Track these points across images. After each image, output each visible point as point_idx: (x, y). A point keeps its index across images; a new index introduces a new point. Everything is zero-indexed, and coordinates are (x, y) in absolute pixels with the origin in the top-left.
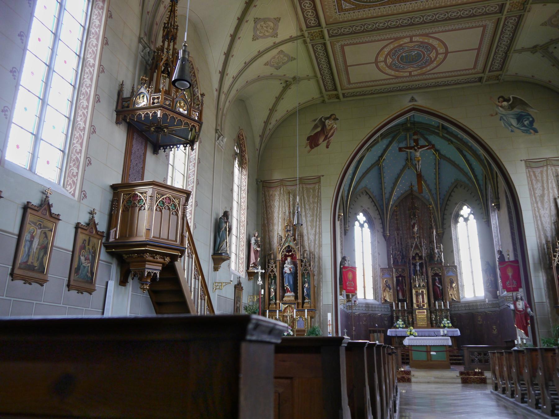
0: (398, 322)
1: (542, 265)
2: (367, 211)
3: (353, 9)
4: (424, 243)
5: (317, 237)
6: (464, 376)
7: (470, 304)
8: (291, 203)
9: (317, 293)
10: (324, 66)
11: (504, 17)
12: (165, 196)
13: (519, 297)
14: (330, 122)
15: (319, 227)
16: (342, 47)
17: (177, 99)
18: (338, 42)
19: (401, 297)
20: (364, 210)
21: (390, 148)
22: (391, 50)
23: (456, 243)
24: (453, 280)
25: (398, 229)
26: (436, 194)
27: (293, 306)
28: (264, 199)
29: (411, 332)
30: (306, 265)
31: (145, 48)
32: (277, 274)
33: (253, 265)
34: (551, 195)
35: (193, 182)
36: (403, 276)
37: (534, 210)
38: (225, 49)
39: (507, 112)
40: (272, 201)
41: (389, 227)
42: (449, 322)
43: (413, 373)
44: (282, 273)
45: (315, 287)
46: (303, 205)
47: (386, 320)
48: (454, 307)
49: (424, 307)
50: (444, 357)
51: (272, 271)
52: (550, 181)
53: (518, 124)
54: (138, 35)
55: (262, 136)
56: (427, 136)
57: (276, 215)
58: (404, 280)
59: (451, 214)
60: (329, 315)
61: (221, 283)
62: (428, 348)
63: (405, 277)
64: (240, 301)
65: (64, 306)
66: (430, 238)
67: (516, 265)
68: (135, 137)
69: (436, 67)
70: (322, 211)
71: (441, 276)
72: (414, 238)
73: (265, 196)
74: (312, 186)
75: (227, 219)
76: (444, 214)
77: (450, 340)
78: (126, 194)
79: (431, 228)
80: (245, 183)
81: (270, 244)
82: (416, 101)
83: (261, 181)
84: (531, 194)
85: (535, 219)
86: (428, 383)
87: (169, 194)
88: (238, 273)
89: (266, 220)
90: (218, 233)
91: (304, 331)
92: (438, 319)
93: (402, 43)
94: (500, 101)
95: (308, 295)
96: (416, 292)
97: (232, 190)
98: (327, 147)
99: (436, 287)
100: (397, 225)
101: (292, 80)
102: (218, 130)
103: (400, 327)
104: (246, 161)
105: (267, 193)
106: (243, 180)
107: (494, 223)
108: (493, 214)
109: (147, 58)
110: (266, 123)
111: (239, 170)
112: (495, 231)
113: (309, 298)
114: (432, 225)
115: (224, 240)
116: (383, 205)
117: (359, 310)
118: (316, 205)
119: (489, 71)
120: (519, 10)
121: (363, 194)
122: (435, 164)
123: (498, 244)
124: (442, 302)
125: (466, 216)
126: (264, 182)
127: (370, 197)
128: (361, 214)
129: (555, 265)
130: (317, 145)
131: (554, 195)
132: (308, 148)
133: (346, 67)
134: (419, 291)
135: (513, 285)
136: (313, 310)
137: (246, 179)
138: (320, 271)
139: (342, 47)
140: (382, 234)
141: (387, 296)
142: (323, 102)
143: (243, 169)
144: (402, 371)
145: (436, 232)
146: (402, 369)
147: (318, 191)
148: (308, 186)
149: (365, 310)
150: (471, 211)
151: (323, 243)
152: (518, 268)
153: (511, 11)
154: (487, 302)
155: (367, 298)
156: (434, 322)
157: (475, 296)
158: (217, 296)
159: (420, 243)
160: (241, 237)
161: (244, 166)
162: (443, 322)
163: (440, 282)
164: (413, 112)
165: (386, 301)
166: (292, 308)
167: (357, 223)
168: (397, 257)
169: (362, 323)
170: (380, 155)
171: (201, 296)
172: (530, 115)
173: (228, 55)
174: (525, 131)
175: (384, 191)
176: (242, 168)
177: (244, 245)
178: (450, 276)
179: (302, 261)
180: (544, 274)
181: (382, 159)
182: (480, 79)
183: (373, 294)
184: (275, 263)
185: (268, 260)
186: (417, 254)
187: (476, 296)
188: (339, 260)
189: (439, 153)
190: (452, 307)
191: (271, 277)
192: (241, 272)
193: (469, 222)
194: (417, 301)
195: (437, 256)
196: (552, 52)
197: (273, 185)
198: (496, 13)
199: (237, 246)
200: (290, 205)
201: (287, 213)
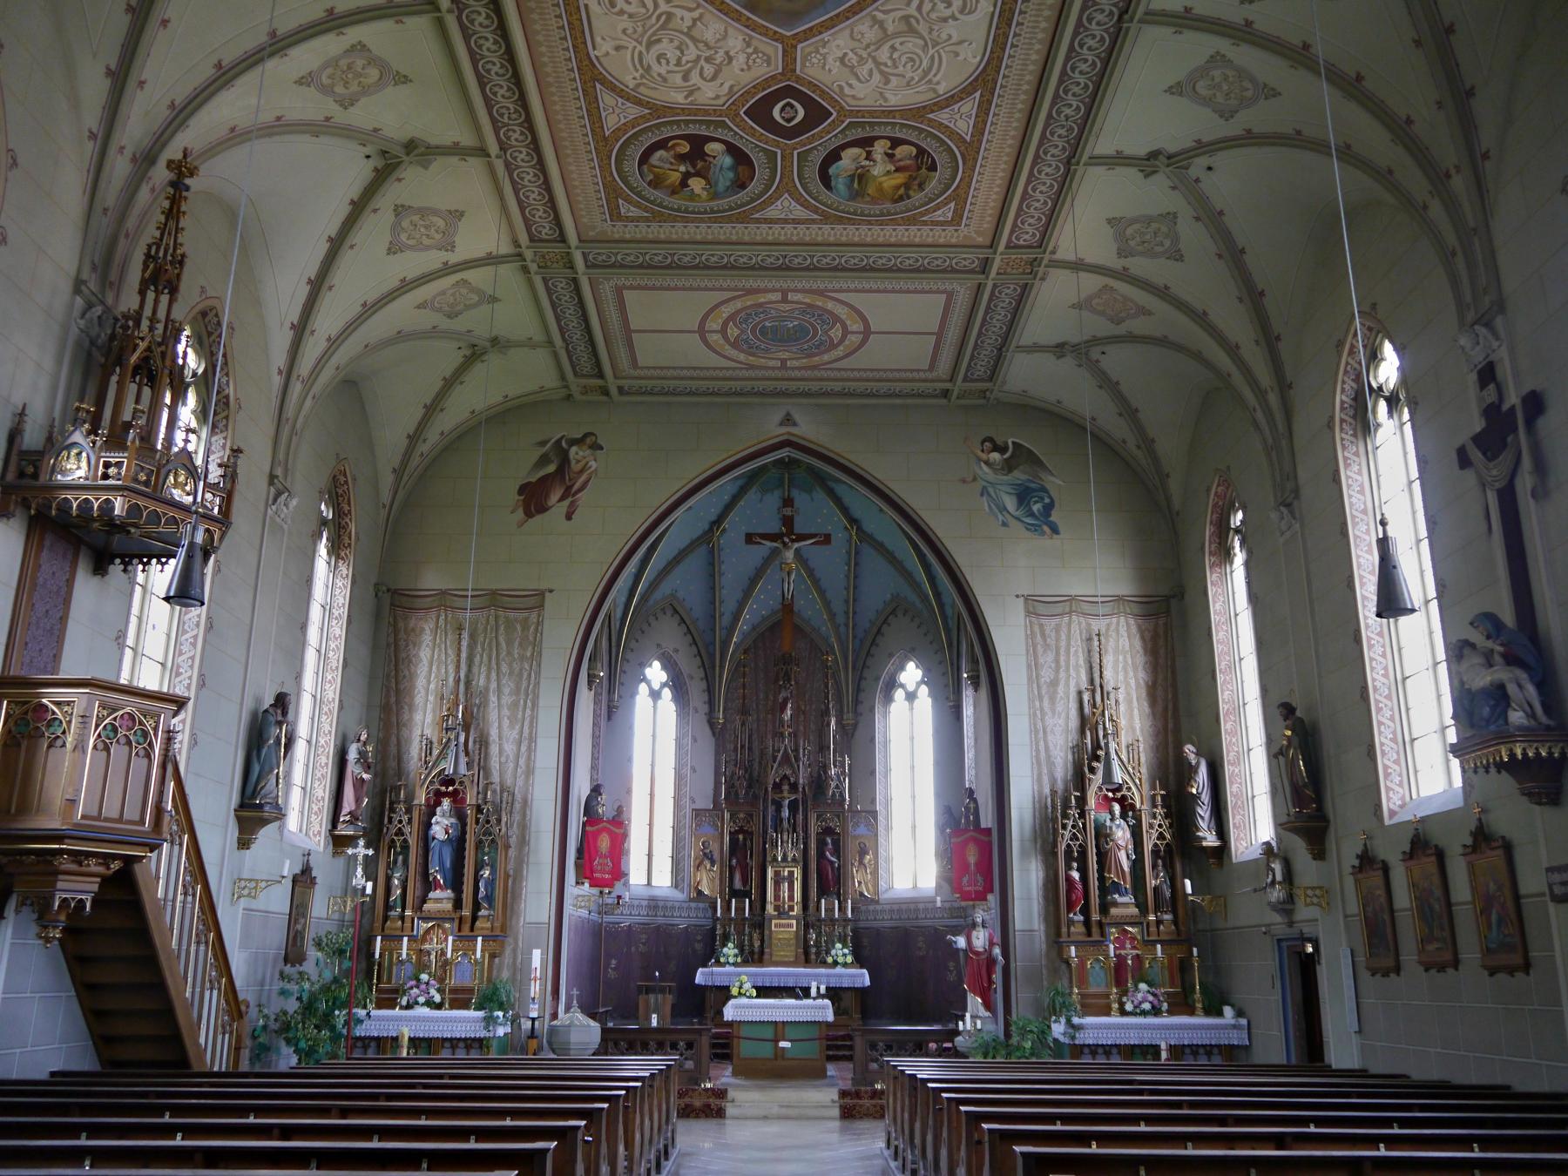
0: (725, 950)
3: (647, 220)
5: (523, 749)
6: (848, 1101)
8: (464, 655)
9: (513, 892)
10: (573, 322)
11: (990, 284)
12: (121, 713)
13: (979, 920)
14: (581, 453)
15: (531, 723)
16: (619, 291)
17: (170, 466)
18: (608, 280)
19: (738, 885)
20: (663, 654)
21: (742, 503)
22: (738, 312)
25: (744, 711)
26: (847, 625)
27: (447, 925)
28: (391, 640)
29: (740, 988)
30: (488, 822)
31: (89, 306)
32: (412, 841)
33: (347, 818)
34: (1072, 684)
35: (198, 625)
37: (1033, 716)
38: (312, 272)
40: (415, 645)
41: (725, 702)
42: (846, 951)
43: (731, 1094)
44: (426, 838)
45: (507, 876)
46: (494, 662)
47: (699, 941)
50: (813, 1050)
51: (400, 832)
52: (1072, 650)
54: (73, 270)
55: (398, 473)
57: (420, 682)
58: (748, 843)
59: (878, 679)
60: (537, 955)
61: (257, 881)
62: (779, 1029)
63: (752, 833)
64: (304, 916)
66: (820, 736)
68: (47, 543)
69: (847, 356)
70: (542, 680)
72: (782, 735)
73: (396, 632)
74: (521, 615)
75: (285, 714)
76: (861, 678)
78: (17, 703)
79: (826, 713)
80: (342, 598)
81: (399, 759)
82: (795, 424)
83: (388, 590)
86: (765, 1118)
87: (130, 706)
88: (307, 839)
89: (393, 694)
90: (255, 753)
91: (470, 991)
93: (762, 300)
95: (490, 898)
96: (777, 874)
97: (304, 627)
98: (569, 517)
101: (488, 344)
102: (277, 477)
104: (350, 538)
105: (401, 624)
106: (338, 591)
109: (95, 331)
110: (414, 439)
111: (329, 563)
113: (491, 906)
115: (271, 771)
116: (714, 644)
118: (527, 666)
119: (965, 380)
120: (1024, 273)
122: (849, 553)
125: (911, 688)
126: (394, 593)
130: (543, 509)
131: (1077, 684)
132: (520, 513)
133: (628, 331)
136: (497, 939)
137: (346, 587)
138: (524, 837)
139: (619, 291)
140: (704, 719)
141: (705, 882)
142: (569, 397)
143: (341, 562)
144: (707, 1090)
146: (709, 1085)
147: (536, 630)
148: (512, 615)
150: (924, 676)
151: (538, 765)
152: (990, 844)
153: (1005, 273)
154: (939, 904)
156: (813, 950)
157: (915, 887)
158: (241, 911)
159: (796, 750)
160: (322, 742)
161: (343, 554)
162: (833, 952)
163: (837, 851)
164: (787, 449)
165: (700, 893)
166: (444, 932)
167: (643, 688)
168: (737, 784)
170: (714, 518)
171: (197, 935)
172: (1046, 491)
173: (318, 285)
176: (338, 557)
177: (327, 764)
179: (479, 810)
180: (1040, 866)
182: (946, 394)
184: (409, 811)
185: (392, 803)
186: (785, 777)
188: (581, 787)
191: (395, 847)
192: (315, 835)
193: (917, 702)
194: (777, 897)
195: (833, 784)
196: (1097, 361)
197: (419, 603)
198: (972, 271)
199: (307, 766)
200: (459, 661)
201: (451, 679)
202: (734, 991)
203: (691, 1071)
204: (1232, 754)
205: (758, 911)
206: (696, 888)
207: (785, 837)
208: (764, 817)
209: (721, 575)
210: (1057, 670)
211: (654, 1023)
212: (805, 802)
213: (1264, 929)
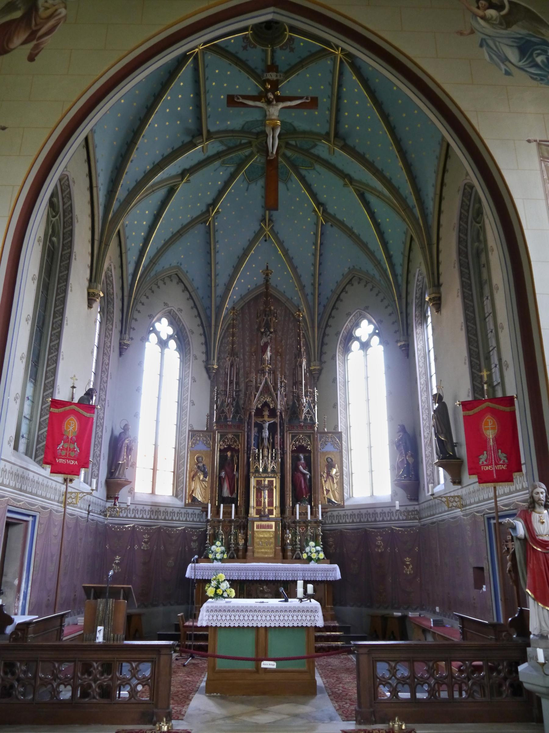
0: (213, 548)
2: (176, 314)
4: (281, 382)
7: (362, 511)
19: (226, 493)
20: (170, 312)
23: (343, 391)
24: (332, 460)
25: (233, 353)
26: (313, 294)
29: (217, 588)
36: (234, 448)
39: (495, 31)
41: (219, 353)
42: (319, 548)
48: (332, 516)
49: (270, 516)
53: (520, 61)
56: (304, 172)
59: (338, 334)
67: (508, 409)
71: (309, 452)
72: (263, 372)
76: (324, 334)
77: (320, 613)
79: (299, 355)
92: (297, 540)
94: (480, 5)
96: (259, 483)
98: (31, 58)
99: (299, 474)
100: (233, 346)
103: (216, 559)
107: (419, 347)
108: (418, 331)
112: (421, 364)
114: (300, 351)
116: (210, 308)
117: (135, 517)
121: (171, 280)
122: (316, 234)
123: (425, 389)
124: (309, 506)
125: (364, 339)
127: (186, 288)
128: (165, 321)
134: (264, 481)
140: (203, 365)
145: (309, 364)
149: (150, 518)
150: (376, 329)
154: (398, 508)
155: (157, 492)
156: (290, 548)
157: (372, 495)
162: (307, 549)
163: (308, 465)
164: (271, 9)
165: (194, 499)
167: (153, 337)
168: (226, 410)
169: (140, 546)
170: (210, 201)
174: (539, 78)
175: (215, 279)
178: (329, 453)
181: (213, 211)
183: (173, 484)
186: (266, 404)
187: (374, 494)
189: (325, 211)
190: (327, 516)
193: (370, 350)
194: (259, 503)
195: (305, 410)
202: (210, 591)
203: (145, 703)
205: (242, 514)
206: (191, 495)
207: (266, 453)
208: (249, 437)
209: (216, 252)
211: (100, 638)
212: (282, 424)
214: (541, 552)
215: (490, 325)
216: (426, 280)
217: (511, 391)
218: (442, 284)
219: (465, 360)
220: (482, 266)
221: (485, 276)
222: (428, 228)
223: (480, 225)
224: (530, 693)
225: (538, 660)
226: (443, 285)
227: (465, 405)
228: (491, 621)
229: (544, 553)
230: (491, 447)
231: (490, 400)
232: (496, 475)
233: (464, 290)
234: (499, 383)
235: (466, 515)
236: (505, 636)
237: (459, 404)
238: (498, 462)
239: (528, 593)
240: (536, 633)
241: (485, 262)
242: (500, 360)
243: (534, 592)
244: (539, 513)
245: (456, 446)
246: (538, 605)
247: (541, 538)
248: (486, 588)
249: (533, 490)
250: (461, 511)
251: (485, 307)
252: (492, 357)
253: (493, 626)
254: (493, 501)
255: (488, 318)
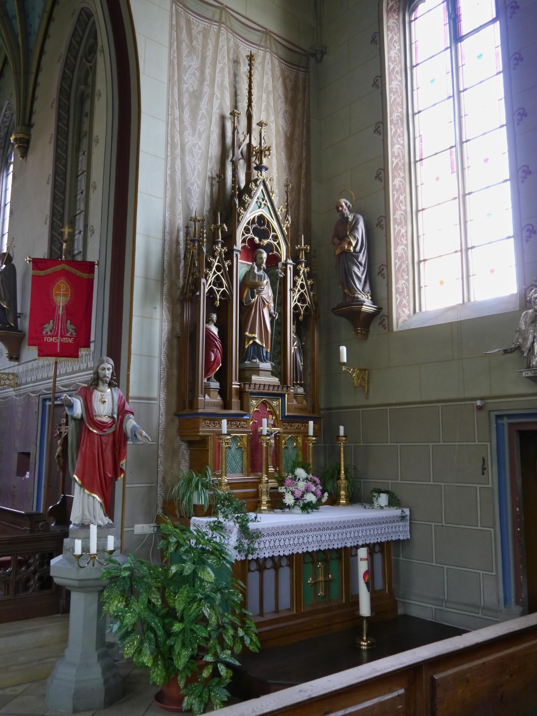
1: (165, 287)
37: (170, 125)
52: (219, 66)
65: (395, 444)
67: (85, 276)
84: (173, 75)
85: (169, 150)
129: (206, 290)
131: (221, 107)
135: (62, 336)
180: (166, 316)
204: (399, 213)
210: (202, 80)
213: (479, 403)
214: (97, 434)
215: (82, 185)
216: (15, 117)
217: (92, 256)
218: (33, 125)
219: (46, 219)
220: (85, 114)
221: (85, 127)
222: (28, 51)
223: (91, 64)
224: (59, 588)
225: (74, 552)
226: (34, 127)
227: (37, 263)
228: (29, 511)
229: (100, 435)
230: (59, 316)
231: (67, 262)
232: (60, 348)
233: (59, 137)
234: (80, 252)
235: (20, 395)
236: (41, 526)
237: (29, 261)
238: (65, 334)
239: (75, 480)
240: (77, 522)
241: (88, 130)
242: (86, 226)
243: (81, 478)
244: (102, 391)
245: (19, 317)
246: (84, 491)
247: (99, 419)
248: (30, 475)
249: (100, 365)
250: (14, 390)
251: (76, 242)
252: (77, 222)
253: (30, 516)
254: (52, 380)
255: (81, 176)
